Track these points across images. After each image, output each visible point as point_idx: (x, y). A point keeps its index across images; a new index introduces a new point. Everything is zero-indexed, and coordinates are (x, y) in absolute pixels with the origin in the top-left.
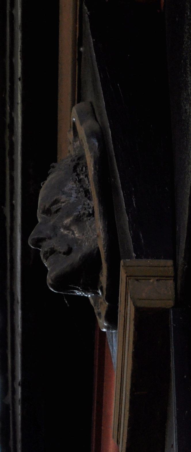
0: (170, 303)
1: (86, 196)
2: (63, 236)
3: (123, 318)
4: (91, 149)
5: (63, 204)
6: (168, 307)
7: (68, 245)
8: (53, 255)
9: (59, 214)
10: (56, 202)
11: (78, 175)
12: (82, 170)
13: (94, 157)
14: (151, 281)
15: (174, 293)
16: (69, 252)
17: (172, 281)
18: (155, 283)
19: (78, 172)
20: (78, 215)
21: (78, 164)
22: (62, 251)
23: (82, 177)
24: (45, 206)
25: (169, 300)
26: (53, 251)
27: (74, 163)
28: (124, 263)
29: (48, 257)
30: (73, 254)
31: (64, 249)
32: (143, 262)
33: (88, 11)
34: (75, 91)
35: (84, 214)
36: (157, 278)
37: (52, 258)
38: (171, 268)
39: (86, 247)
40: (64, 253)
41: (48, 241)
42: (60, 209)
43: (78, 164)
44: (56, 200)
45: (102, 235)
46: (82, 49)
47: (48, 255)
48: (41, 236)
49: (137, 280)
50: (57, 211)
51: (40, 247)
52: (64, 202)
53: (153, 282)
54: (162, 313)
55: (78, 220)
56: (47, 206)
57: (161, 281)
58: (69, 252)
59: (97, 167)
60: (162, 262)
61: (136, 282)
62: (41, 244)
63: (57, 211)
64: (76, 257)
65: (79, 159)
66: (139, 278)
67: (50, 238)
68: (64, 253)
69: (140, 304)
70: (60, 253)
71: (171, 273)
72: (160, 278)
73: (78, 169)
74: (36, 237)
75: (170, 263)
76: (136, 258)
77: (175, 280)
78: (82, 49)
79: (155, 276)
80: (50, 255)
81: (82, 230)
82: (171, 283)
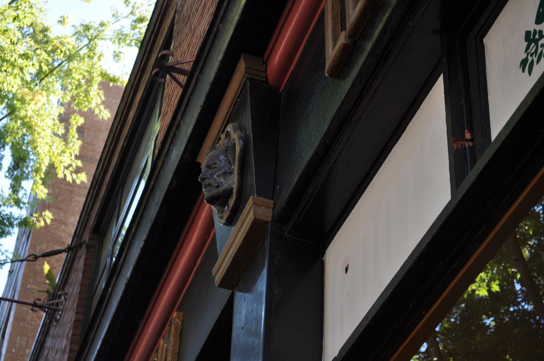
0: (270, 219)
1: (229, 164)
2: (215, 179)
3: (243, 221)
4: (239, 144)
5: (218, 165)
6: (269, 221)
7: (218, 183)
8: (209, 187)
9: (215, 169)
10: (215, 164)
11: (227, 154)
12: (229, 152)
13: (240, 148)
14: (263, 208)
15: (272, 215)
16: (218, 187)
17: (271, 210)
18: (265, 209)
19: (227, 153)
20: (225, 172)
21: (228, 149)
22: (215, 186)
23: (228, 155)
24: (209, 164)
25: (270, 218)
26: (210, 185)
27: (226, 149)
28: (253, 197)
29: (206, 187)
30: (219, 188)
31: (216, 185)
32: (261, 198)
33: (249, 84)
34: (227, 117)
35: (227, 172)
36: (265, 207)
37: (208, 188)
38: (272, 204)
39: (226, 186)
40: (216, 187)
41: (208, 180)
42: (215, 167)
43: (228, 149)
44: (215, 163)
45: (236, 183)
46: (238, 100)
47: (207, 186)
48: (205, 177)
49: (257, 206)
50: (215, 167)
51: (203, 182)
52: (218, 165)
53: (264, 208)
54: (267, 222)
55: (225, 174)
56: (210, 164)
57: (267, 209)
58: (218, 187)
59: (241, 153)
60: (269, 201)
61: (256, 207)
62: (204, 180)
63: (215, 167)
64: (221, 189)
65: (228, 147)
66: (258, 205)
67: (209, 179)
68: (216, 187)
69: (257, 217)
70: (213, 186)
71: (272, 206)
72: (267, 207)
73: (227, 152)
74: (203, 177)
75: (272, 202)
76: (257, 196)
77: (273, 209)
78: (238, 100)
79: (265, 206)
80: (208, 186)
81: (225, 179)
82: (271, 210)
